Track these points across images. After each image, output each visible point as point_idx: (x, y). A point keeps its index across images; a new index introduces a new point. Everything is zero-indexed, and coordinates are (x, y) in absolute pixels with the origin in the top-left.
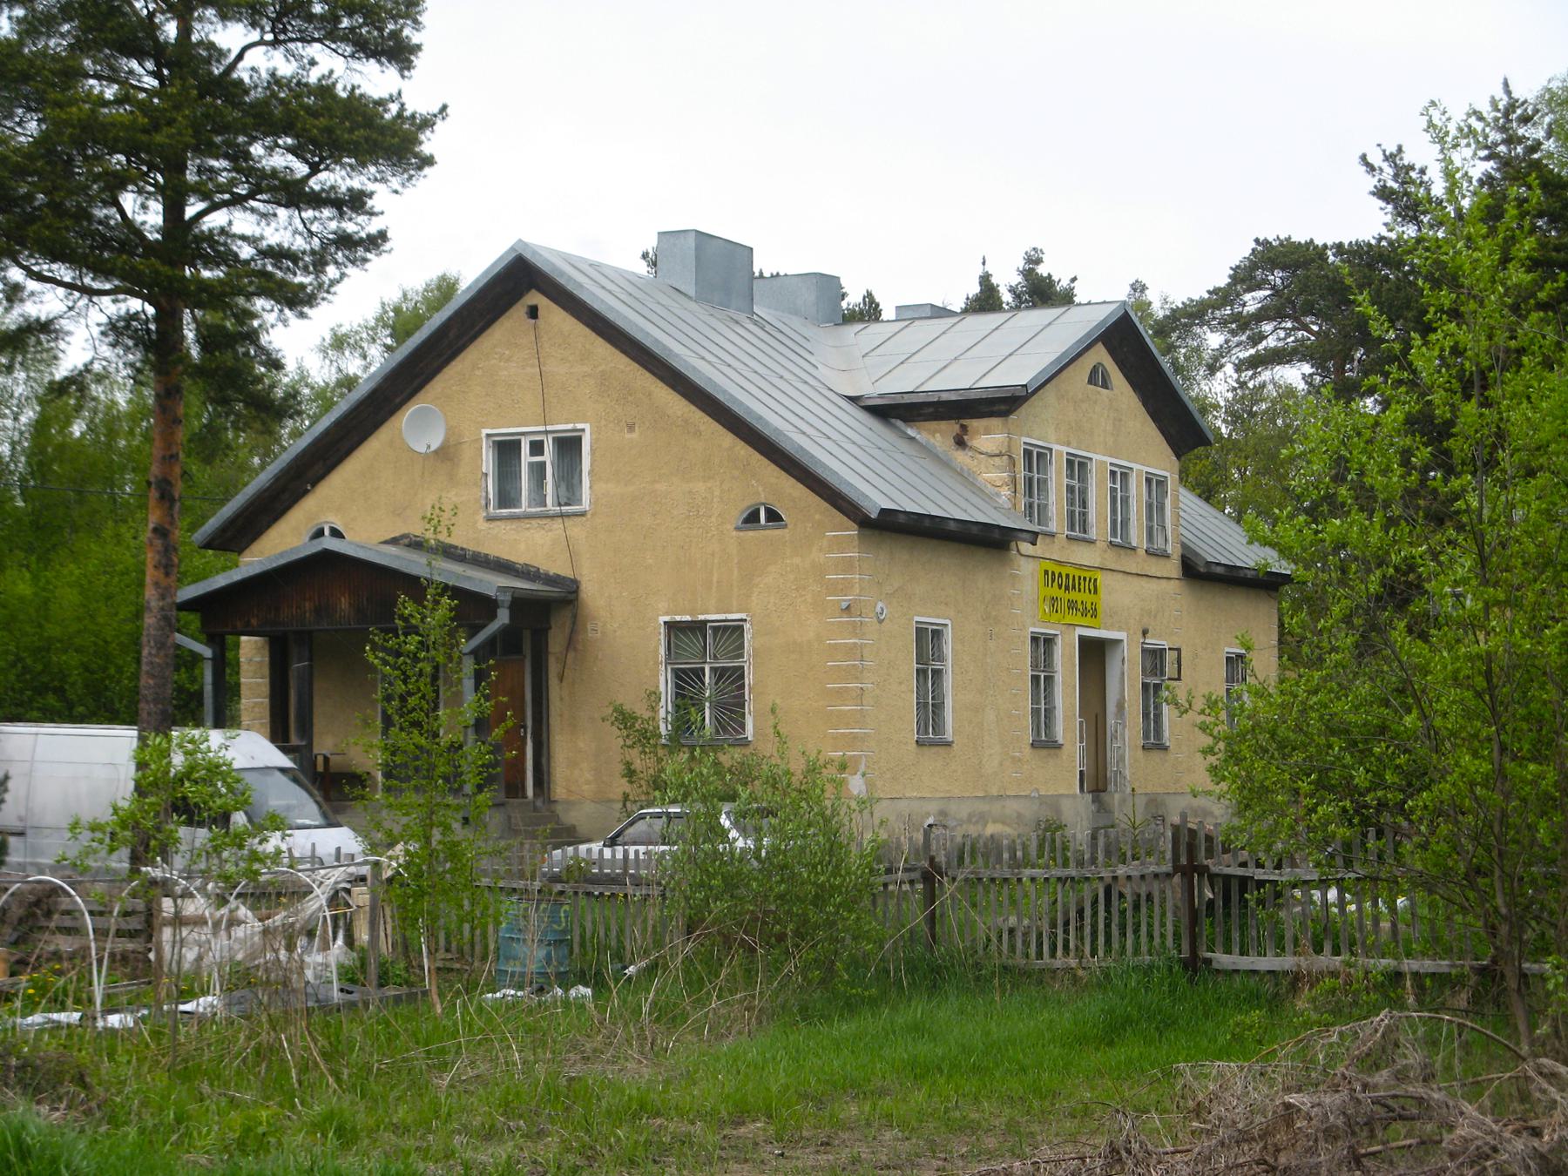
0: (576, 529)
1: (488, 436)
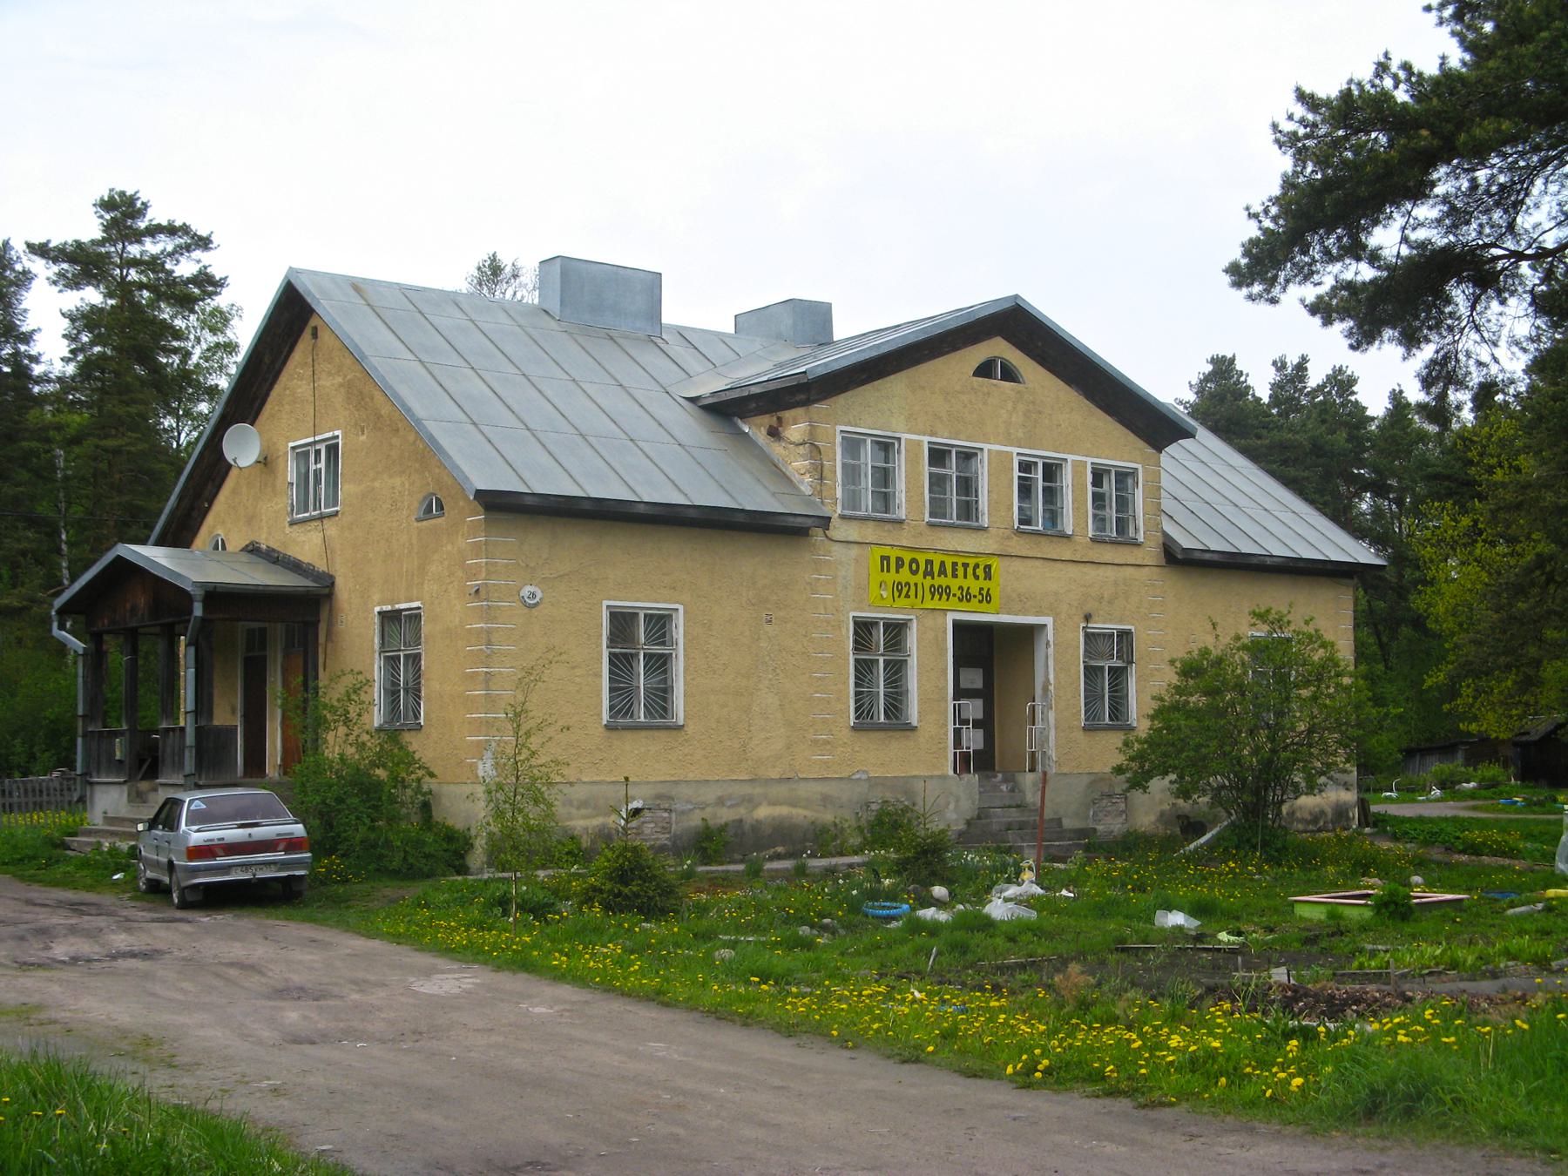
0: (331, 528)
1: (293, 448)
